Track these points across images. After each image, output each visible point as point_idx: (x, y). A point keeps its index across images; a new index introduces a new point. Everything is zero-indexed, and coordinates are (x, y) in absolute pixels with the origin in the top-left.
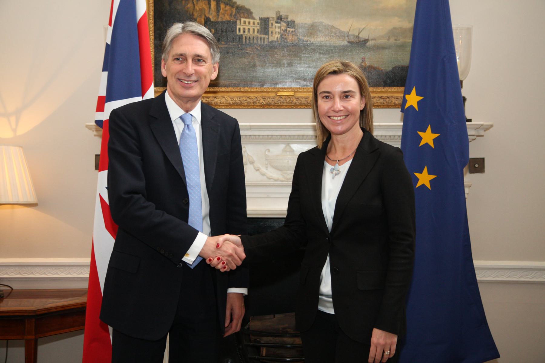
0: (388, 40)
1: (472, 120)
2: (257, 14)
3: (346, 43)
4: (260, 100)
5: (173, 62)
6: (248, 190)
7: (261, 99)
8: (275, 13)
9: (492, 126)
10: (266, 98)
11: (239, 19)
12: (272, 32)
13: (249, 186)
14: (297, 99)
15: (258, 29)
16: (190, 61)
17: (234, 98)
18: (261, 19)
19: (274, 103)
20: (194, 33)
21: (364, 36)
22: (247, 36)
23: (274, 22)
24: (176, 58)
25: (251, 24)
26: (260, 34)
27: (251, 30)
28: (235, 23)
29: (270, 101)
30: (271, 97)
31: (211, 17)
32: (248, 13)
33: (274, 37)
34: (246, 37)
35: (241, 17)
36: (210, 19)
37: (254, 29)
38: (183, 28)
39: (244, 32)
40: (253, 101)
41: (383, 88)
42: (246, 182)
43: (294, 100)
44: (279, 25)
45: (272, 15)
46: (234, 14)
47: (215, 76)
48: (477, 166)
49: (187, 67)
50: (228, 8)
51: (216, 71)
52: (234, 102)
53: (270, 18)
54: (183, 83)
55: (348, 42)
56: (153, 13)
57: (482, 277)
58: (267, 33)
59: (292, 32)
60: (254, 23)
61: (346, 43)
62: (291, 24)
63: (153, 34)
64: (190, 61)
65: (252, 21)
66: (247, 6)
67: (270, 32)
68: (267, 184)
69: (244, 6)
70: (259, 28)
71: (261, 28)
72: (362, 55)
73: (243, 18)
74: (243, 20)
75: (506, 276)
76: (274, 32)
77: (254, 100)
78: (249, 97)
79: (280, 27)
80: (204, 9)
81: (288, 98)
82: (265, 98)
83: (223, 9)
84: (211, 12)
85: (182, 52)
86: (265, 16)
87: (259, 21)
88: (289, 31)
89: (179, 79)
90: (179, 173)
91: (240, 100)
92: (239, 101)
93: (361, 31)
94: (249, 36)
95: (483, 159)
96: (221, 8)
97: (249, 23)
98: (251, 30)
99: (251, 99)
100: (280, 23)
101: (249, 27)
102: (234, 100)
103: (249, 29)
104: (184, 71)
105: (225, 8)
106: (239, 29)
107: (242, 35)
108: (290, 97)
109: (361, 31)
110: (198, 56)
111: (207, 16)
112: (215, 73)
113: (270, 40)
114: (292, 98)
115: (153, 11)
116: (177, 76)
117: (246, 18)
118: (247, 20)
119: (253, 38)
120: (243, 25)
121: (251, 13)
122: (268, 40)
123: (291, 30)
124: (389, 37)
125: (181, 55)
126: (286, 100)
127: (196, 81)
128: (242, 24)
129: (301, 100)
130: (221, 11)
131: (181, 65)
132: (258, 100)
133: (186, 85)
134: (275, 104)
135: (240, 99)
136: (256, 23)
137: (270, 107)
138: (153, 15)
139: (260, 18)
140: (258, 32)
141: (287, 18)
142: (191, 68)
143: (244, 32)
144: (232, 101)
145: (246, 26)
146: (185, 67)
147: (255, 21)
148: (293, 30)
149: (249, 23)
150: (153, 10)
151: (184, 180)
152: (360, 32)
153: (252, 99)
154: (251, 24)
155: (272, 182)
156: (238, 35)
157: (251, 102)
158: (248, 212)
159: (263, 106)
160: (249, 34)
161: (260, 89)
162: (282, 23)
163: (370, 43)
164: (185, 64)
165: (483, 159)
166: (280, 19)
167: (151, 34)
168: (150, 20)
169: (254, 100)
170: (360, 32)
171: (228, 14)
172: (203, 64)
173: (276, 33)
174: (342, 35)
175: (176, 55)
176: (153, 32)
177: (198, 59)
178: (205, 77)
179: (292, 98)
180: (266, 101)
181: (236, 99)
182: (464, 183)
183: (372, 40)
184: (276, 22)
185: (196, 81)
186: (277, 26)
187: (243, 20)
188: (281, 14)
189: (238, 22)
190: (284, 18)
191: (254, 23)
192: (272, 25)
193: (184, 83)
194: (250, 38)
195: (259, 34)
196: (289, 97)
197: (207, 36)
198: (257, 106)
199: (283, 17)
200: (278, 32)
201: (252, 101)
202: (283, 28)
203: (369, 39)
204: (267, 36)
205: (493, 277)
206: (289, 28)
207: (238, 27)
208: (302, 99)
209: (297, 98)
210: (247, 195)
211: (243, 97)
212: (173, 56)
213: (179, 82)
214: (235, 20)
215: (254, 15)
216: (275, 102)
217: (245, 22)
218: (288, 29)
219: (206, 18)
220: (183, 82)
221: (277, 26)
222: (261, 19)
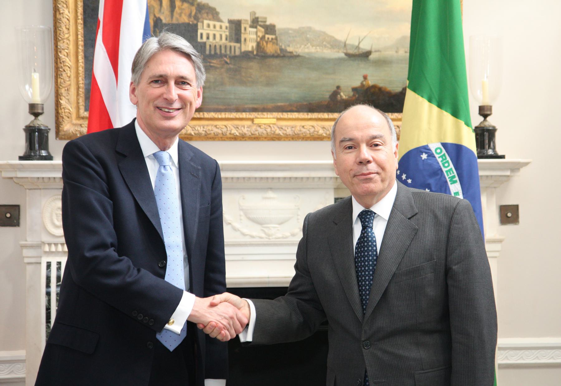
0: (397, 52)
1: (506, 157)
2: (226, 15)
3: (342, 55)
4: (232, 129)
5: (148, 86)
6: (227, 250)
7: (233, 128)
8: (249, 13)
9: (526, 164)
10: (240, 128)
11: (201, 22)
12: (245, 40)
13: (229, 245)
14: (280, 129)
15: (227, 36)
16: (172, 83)
17: (196, 127)
18: (230, 22)
19: (250, 134)
20: (176, 50)
21: (365, 46)
22: (212, 45)
23: (248, 26)
24: (155, 81)
25: (218, 28)
26: (230, 41)
27: (218, 37)
28: (196, 26)
29: (245, 130)
30: (246, 126)
31: (162, 18)
32: (213, 14)
33: (248, 46)
34: (210, 46)
35: (204, 19)
36: (161, 20)
37: (221, 36)
38: (159, 42)
39: (208, 38)
40: (222, 131)
41: (392, 115)
42: (225, 240)
43: (276, 130)
44: (255, 30)
45: (245, 16)
46: (193, 13)
47: (200, 104)
48: (509, 215)
49: (169, 91)
50: (186, 5)
51: (200, 97)
52: (197, 132)
53: (243, 22)
54: (164, 112)
55: (346, 54)
56: (82, 10)
57: (519, 359)
58: (238, 40)
59: (272, 39)
60: (221, 27)
61: (342, 55)
62: (270, 29)
63: (83, 39)
64: (172, 83)
65: (218, 24)
66: (212, 4)
67: (243, 40)
68: (242, 243)
69: (208, 4)
70: (228, 33)
71: (230, 33)
72: (365, 72)
73: (206, 19)
74: (206, 22)
75: (548, 357)
76: (248, 39)
77: (223, 130)
78: (216, 126)
79: (256, 33)
80: (153, 6)
81: (268, 127)
82: (238, 127)
83: (179, 7)
84: (162, 11)
85: (162, 73)
86: (236, 17)
87: (228, 25)
88: (268, 38)
89: (158, 108)
90: (156, 227)
91: (204, 130)
92: (203, 131)
93: (362, 40)
94: (214, 44)
95: (517, 207)
96: (177, 6)
97: (215, 27)
98: (218, 37)
99: (218, 128)
100: (256, 27)
101: (221, 33)
102: (195, 129)
103: (214, 35)
104: (165, 96)
105: (182, 5)
106: (202, 34)
107: (205, 43)
108: (271, 125)
109: (362, 40)
110: (182, 78)
111: (157, 15)
112: (199, 99)
113: (243, 50)
114: (274, 127)
115: (82, 8)
116: (156, 102)
117: (210, 20)
118: (212, 23)
119: (221, 46)
120: (206, 30)
121: (218, 13)
122: (241, 50)
123: (271, 37)
124: (397, 48)
125: (161, 76)
126: (266, 130)
127: (179, 109)
128: (205, 27)
129: (285, 130)
130: (177, 9)
131: (161, 88)
132: (229, 129)
133: (167, 113)
134: (252, 134)
135: (204, 128)
136: (224, 27)
137: (244, 139)
138: (82, 13)
139: (228, 20)
140: (226, 39)
141: (265, 22)
142: (175, 92)
143: (208, 38)
144: (194, 132)
145: (211, 30)
146: (165, 91)
147: (222, 24)
148: (274, 37)
149: (215, 27)
150: (82, 6)
151: (161, 236)
152: (361, 40)
153: (220, 128)
154: (218, 28)
155: (247, 239)
156: (200, 43)
157: (219, 133)
158: (227, 281)
159: (235, 138)
160: (214, 41)
161: (230, 116)
162: (259, 27)
163: (372, 57)
164: (166, 86)
165: (517, 207)
166: (255, 22)
167: (80, 38)
168: (79, 19)
169: (222, 130)
170: (361, 40)
171: (185, 14)
172: (188, 87)
173: (251, 40)
174: (334, 44)
175: (154, 76)
176: (83, 36)
177: (181, 82)
178: (191, 104)
179: (274, 127)
180: (239, 131)
181: (199, 129)
182: (224, 242)
183: (376, 51)
184: (251, 27)
185: (179, 109)
186: (252, 32)
187: (206, 22)
188: (257, 16)
189: (200, 25)
190: (262, 22)
191: (221, 27)
192: (245, 29)
193: (165, 111)
194: (221, 46)
195: (228, 42)
196: (270, 126)
197: (192, 53)
198: (227, 138)
199: (260, 20)
200: (254, 40)
201: (220, 132)
202: (260, 34)
203: (373, 50)
204: (237, 45)
205: (532, 359)
206: (267, 34)
207: (200, 31)
208: (286, 129)
209: (279, 127)
210: (227, 258)
211: (207, 126)
212: (150, 78)
213: (158, 110)
214: (195, 22)
215: (221, 16)
216: (251, 133)
217: (209, 26)
218: (267, 36)
219: (155, 19)
220: (163, 111)
221: (252, 32)
222: (230, 22)
